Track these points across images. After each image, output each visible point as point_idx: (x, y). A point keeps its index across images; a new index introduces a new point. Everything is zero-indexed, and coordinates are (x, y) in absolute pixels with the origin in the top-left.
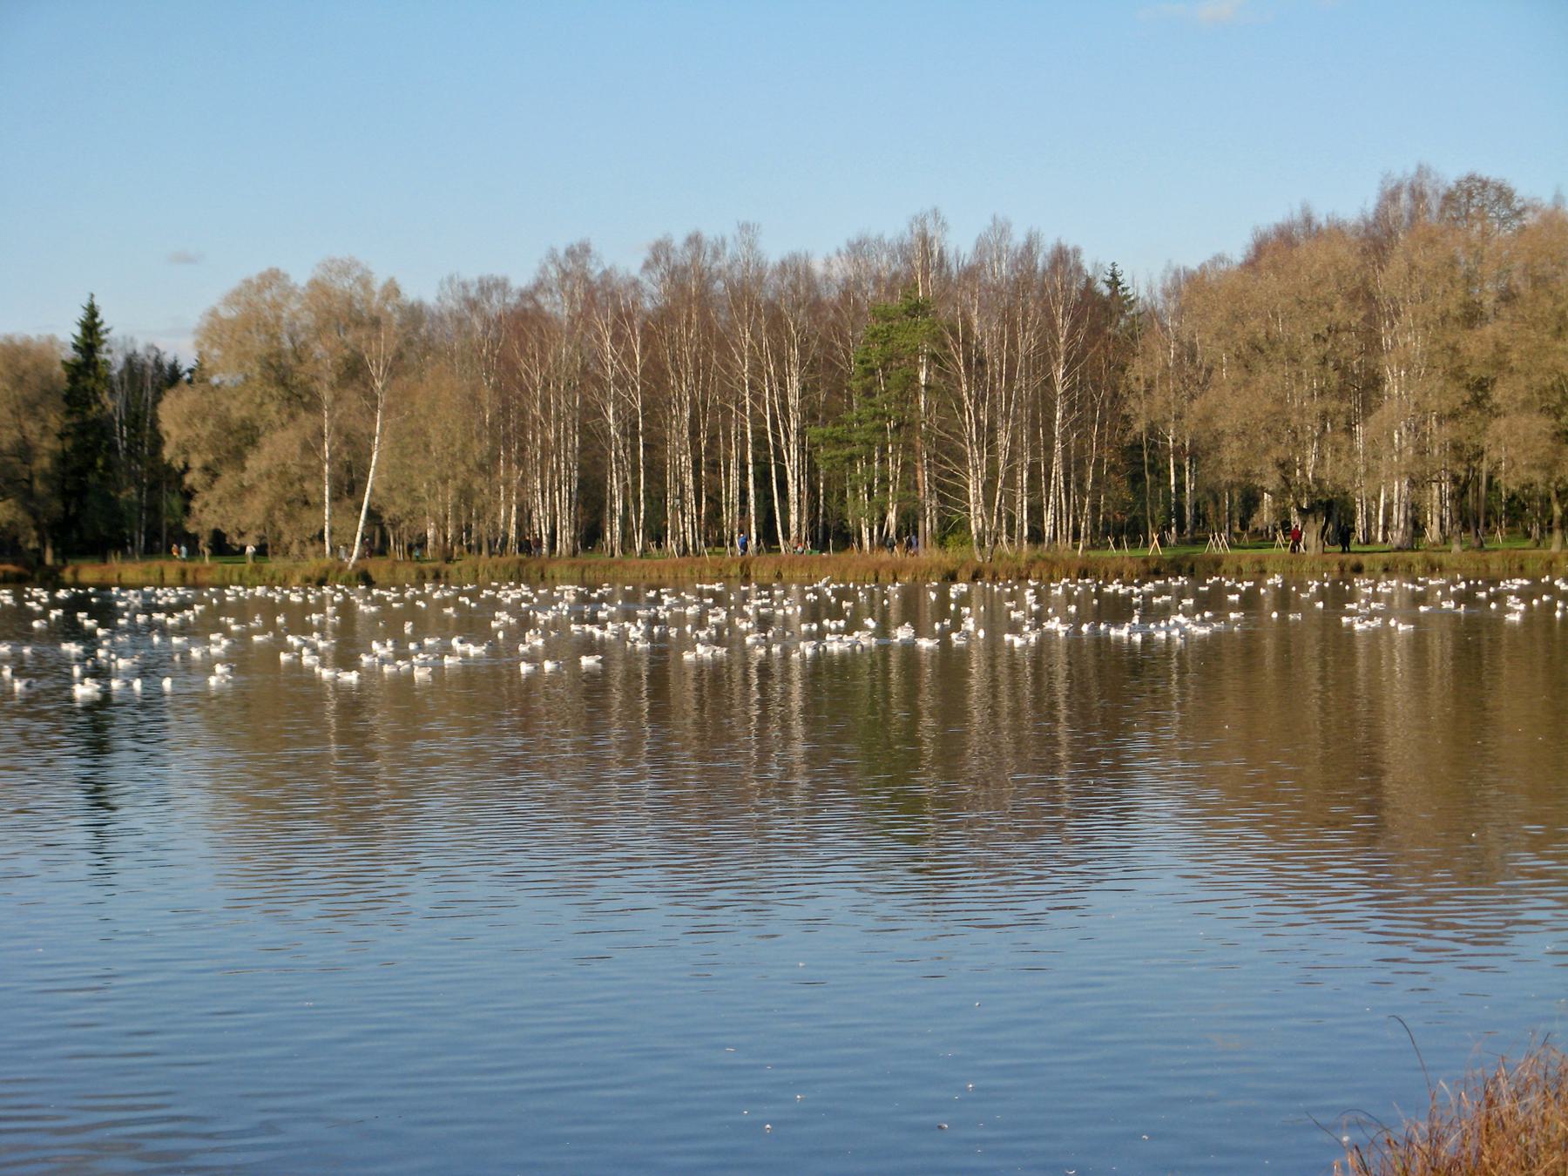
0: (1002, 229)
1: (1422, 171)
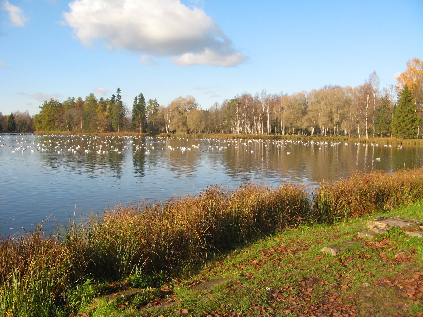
0: (282, 93)
1: (330, 85)
